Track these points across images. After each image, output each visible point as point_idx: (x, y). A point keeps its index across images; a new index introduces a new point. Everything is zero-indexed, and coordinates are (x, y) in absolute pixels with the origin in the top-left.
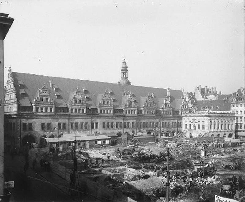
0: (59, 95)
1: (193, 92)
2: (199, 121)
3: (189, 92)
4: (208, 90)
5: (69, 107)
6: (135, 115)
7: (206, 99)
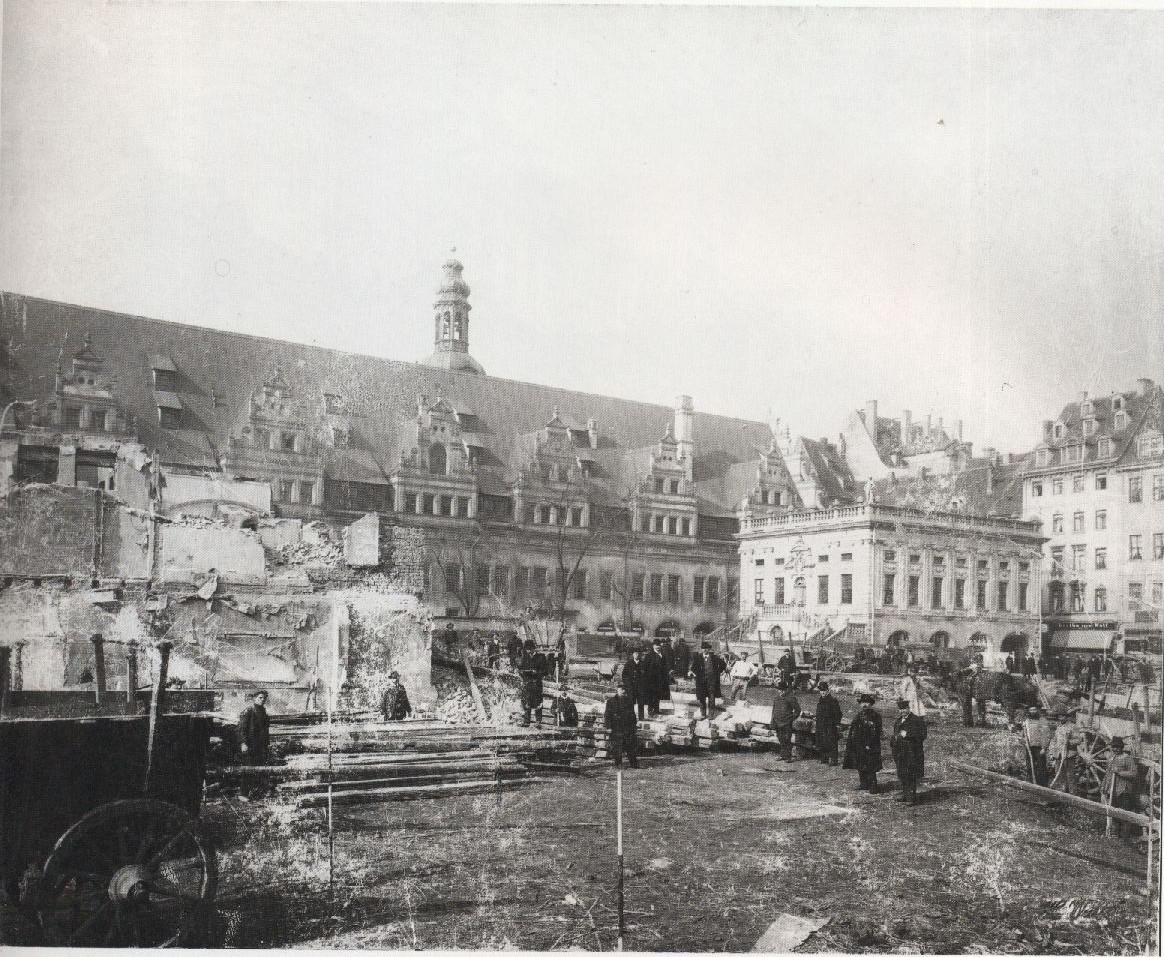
0: (475, 443)
1: (834, 440)
2: (824, 558)
3: (817, 439)
4: (916, 431)
5: (396, 487)
6: (446, 522)
7: (900, 472)
